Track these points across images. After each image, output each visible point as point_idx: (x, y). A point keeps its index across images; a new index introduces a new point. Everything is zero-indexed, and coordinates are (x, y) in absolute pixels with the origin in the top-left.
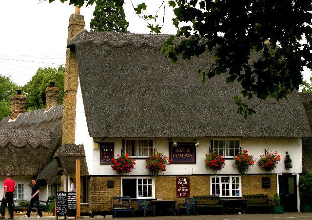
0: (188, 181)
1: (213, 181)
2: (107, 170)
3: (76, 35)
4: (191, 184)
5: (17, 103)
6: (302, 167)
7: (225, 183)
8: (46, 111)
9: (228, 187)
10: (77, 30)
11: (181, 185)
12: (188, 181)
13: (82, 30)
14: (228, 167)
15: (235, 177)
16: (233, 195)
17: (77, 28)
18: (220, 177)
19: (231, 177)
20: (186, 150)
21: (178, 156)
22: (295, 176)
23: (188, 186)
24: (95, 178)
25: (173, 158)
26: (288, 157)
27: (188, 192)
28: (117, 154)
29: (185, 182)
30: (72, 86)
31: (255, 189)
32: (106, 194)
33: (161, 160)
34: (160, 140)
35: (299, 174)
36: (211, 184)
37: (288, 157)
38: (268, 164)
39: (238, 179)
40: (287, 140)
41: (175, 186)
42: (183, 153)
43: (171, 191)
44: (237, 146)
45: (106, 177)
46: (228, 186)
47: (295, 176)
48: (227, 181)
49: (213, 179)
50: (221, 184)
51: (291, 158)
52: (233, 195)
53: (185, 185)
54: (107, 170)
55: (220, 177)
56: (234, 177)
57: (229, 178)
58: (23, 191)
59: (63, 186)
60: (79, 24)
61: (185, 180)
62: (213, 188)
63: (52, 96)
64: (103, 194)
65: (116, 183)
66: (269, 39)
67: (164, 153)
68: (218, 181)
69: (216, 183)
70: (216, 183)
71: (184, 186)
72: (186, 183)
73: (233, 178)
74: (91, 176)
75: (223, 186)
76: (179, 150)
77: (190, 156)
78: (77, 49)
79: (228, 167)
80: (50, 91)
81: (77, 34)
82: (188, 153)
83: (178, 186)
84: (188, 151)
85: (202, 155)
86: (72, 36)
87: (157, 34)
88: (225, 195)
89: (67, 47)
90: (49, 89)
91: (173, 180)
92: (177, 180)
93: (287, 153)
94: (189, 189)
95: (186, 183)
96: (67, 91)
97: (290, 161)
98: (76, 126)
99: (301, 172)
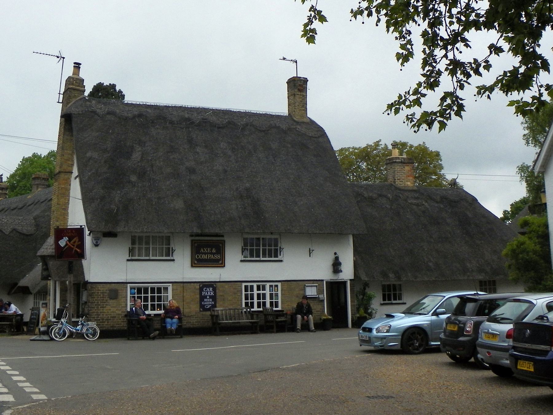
0: (214, 290)
1: (246, 290)
3: (73, 102)
4: (218, 293)
6: (353, 271)
8: (29, 197)
9: (264, 298)
10: (75, 97)
11: (205, 297)
12: (214, 290)
13: (82, 96)
16: (258, 308)
18: (255, 285)
23: (214, 298)
24: (94, 286)
25: (196, 260)
26: (337, 259)
29: (209, 292)
30: (65, 167)
32: (108, 307)
35: (351, 280)
36: (244, 293)
44: (276, 245)
45: (108, 285)
46: (264, 295)
49: (246, 287)
50: (256, 292)
51: (341, 260)
52: (258, 308)
56: (271, 284)
59: (50, 295)
61: (211, 289)
62: (246, 298)
63: (40, 184)
68: (252, 290)
69: (261, 301)
70: (261, 301)
71: (210, 298)
72: (212, 294)
74: (87, 283)
75: (259, 295)
76: (204, 250)
77: (218, 257)
78: (74, 120)
81: (74, 101)
82: (214, 254)
83: (202, 298)
84: (214, 251)
86: (68, 103)
88: (386, 301)
89: (62, 117)
91: (195, 288)
92: (201, 290)
93: (335, 254)
95: (212, 294)
96: (60, 172)
97: (340, 264)
98: (69, 218)
99: (352, 278)
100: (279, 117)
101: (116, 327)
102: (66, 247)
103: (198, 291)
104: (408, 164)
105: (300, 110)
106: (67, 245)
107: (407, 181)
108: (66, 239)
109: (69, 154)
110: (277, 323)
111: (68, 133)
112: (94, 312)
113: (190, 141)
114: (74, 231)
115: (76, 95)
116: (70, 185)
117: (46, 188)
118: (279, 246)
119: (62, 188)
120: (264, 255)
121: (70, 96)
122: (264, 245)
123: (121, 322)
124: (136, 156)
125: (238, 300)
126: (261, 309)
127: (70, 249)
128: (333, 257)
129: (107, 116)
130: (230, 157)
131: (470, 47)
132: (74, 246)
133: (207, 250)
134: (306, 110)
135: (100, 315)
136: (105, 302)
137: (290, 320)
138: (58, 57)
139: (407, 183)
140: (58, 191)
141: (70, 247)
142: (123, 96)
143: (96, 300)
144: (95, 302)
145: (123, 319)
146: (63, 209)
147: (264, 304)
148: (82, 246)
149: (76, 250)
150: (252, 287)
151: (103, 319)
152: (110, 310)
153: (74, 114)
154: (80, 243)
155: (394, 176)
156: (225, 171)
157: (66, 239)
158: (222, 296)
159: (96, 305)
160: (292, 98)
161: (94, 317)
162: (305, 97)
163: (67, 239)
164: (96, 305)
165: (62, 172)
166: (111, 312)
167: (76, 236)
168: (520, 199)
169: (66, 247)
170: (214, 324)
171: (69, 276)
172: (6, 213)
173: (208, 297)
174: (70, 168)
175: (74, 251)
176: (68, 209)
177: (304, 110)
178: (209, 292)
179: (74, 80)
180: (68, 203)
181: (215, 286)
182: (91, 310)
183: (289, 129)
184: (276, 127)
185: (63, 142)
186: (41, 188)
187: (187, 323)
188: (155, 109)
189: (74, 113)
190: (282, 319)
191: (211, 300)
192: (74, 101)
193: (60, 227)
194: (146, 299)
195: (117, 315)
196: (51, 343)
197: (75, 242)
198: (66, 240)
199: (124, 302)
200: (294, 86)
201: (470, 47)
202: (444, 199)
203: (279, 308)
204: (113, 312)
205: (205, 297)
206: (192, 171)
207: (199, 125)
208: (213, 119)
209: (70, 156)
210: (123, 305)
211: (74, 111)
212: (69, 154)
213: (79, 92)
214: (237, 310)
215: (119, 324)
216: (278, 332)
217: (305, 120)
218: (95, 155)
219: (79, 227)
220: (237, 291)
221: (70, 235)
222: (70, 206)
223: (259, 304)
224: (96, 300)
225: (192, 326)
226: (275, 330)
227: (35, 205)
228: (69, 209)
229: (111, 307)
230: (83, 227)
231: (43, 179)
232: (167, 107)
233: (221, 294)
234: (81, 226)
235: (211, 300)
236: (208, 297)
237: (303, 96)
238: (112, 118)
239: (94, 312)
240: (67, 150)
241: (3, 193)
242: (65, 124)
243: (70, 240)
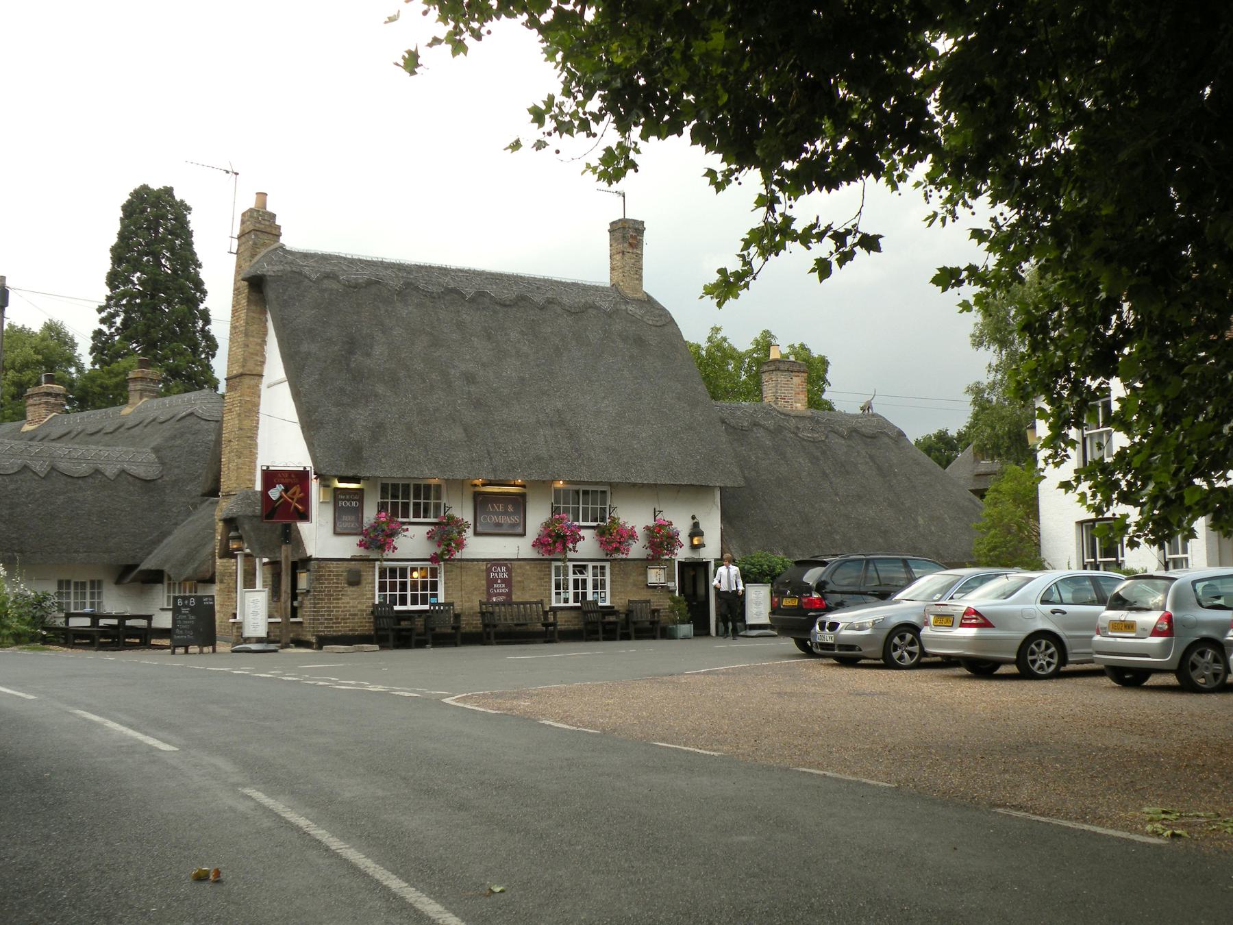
2: (346, 547)
3: (262, 254)
5: (46, 403)
7: (580, 577)
9: (584, 587)
11: (495, 581)
12: (509, 571)
13: (276, 245)
14: (587, 546)
15: (598, 564)
16: (574, 602)
17: (265, 238)
18: (570, 564)
19: (590, 565)
20: (506, 508)
21: (491, 519)
22: (707, 564)
23: (508, 582)
24: (323, 564)
26: (696, 525)
27: (509, 595)
28: (370, 514)
30: (250, 366)
31: (634, 588)
32: (346, 599)
33: (460, 526)
34: (458, 485)
37: (696, 525)
38: (661, 540)
39: (603, 568)
40: (692, 491)
41: (484, 582)
42: (502, 514)
43: (475, 593)
46: (584, 581)
47: (707, 564)
48: (582, 573)
49: (557, 568)
52: (574, 602)
53: (503, 580)
54: (346, 547)
55: (570, 564)
56: (595, 564)
57: (585, 567)
58: (99, 603)
60: (268, 230)
61: (504, 569)
63: (145, 390)
64: (338, 599)
65: (366, 576)
66: (1183, 253)
67: (464, 512)
73: (594, 568)
74: (310, 559)
75: (576, 581)
79: (587, 546)
80: (142, 379)
81: (263, 252)
83: (491, 582)
84: (510, 509)
85: (537, 517)
86: (253, 256)
87: (990, 242)
90: (140, 375)
91: (479, 569)
92: (488, 571)
93: (693, 518)
94: (511, 591)
100: (596, 289)
101: (357, 630)
102: (280, 501)
103: (485, 574)
104: (797, 374)
105: (632, 279)
106: (281, 497)
107: (796, 402)
108: (280, 488)
109: (257, 344)
110: (605, 624)
111: (253, 308)
112: (323, 607)
113: (460, 325)
114: (293, 476)
115: (266, 241)
116: (259, 397)
117: (156, 397)
118: (609, 503)
119: (246, 402)
120: (417, 515)
121: (255, 244)
122: (417, 496)
123: (366, 622)
124: (379, 350)
125: (545, 590)
126: (579, 604)
127: (286, 504)
128: (691, 522)
129: (325, 281)
130: (527, 356)
131: (386, 22)
132: (292, 499)
133: (499, 508)
134: (640, 279)
135: (332, 611)
136: (340, 591)
137: (423, 627)
138: (227, 172)
139: (795, 404)
140: (240, 406)
141: (286, 501)
142: (279, 235)
143: (326, 587)
144: (324, 591)
145: (370, 618)
146: (249, 437)
147: (584, 595)
148: (305, 501)
149: (296, 507)
150: (566, 567)
151: (337, 619)
152: (348, 603)
153: (270, 276)
154: (302, 495)
155: (777, 392)
156: (522, 379)
157: (280, 488)
158: (520, 582)
159: (326, 595)
160: (618, 257)
161: (324, 615)
162: (639, 257)
163: (283, 488)
164: (326, 595)
165: (246, 374)
166: (350, 607)
167: (295, 484)
168: (70, 334)
169: (280, 501)
170: (486, 626)
171: (284, 547)
172: (77, 440)
173: (499, 581)
174: (259, 368)
175: (292, 507)
176: (256, 438)
177: (637, 279)
178: (502, 573)
179: (260, 215)
180: (257, 427)
181: (509, 565)
182: (319, 603)
183: (616, 312)
184: (593, 306)
185: (247, 323)
186: (147, 397)
187: (467, 624)
188: (399, 270)
189: (269, 273)
190: (612, 619)
191: (504, 585)
192: (263, 252)
193: (271, 468)
194: (403, 586)
195: (359, 611)
196: (213, 656)
197: (294, 494)
198: (280, 490)
199: (371, 591)
200: (624, 237)
201: (386, 22)
202: (854, 433)
203: (608, 603)
204: (353, 607)
205: (495, 581)
206: (470, 378)
207: (472, 300)
208: (491, 290)
209: (258, 347)
210: (369, 595)
211: (267, 269)
212: (257, 344)
213: (271, 236)
214: (522, 606)
215: (362, 626)
216: (605, 639)
217: (639, 296)
218: (314, 348)
219: (302, 469)
220: (545, 575)
221: (287, 481)
222: (260, 432)
223: (576, 595)
224: (326, 587)
225: (474, 630)
226: (601, 635)
227: (146, 426)
228: (259, 437)
229: (351, 599)
230: (308, 469)
231: (152, 380)
232: (420, 268)
233: (519, 579)
234: (305, 468)
235: (504, 585)
236: (499, 581)
237: (637, 255)
238: (334, 285)
239: (323, 607)
240: (253, 337)
241: (57, 404)
242: (249, 292)
243: (286, 491)
